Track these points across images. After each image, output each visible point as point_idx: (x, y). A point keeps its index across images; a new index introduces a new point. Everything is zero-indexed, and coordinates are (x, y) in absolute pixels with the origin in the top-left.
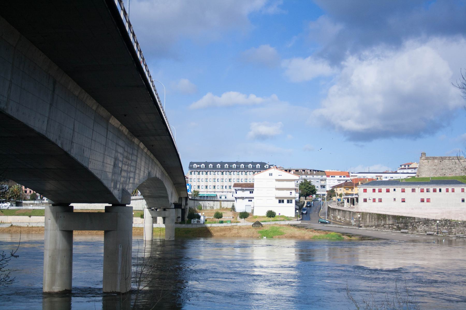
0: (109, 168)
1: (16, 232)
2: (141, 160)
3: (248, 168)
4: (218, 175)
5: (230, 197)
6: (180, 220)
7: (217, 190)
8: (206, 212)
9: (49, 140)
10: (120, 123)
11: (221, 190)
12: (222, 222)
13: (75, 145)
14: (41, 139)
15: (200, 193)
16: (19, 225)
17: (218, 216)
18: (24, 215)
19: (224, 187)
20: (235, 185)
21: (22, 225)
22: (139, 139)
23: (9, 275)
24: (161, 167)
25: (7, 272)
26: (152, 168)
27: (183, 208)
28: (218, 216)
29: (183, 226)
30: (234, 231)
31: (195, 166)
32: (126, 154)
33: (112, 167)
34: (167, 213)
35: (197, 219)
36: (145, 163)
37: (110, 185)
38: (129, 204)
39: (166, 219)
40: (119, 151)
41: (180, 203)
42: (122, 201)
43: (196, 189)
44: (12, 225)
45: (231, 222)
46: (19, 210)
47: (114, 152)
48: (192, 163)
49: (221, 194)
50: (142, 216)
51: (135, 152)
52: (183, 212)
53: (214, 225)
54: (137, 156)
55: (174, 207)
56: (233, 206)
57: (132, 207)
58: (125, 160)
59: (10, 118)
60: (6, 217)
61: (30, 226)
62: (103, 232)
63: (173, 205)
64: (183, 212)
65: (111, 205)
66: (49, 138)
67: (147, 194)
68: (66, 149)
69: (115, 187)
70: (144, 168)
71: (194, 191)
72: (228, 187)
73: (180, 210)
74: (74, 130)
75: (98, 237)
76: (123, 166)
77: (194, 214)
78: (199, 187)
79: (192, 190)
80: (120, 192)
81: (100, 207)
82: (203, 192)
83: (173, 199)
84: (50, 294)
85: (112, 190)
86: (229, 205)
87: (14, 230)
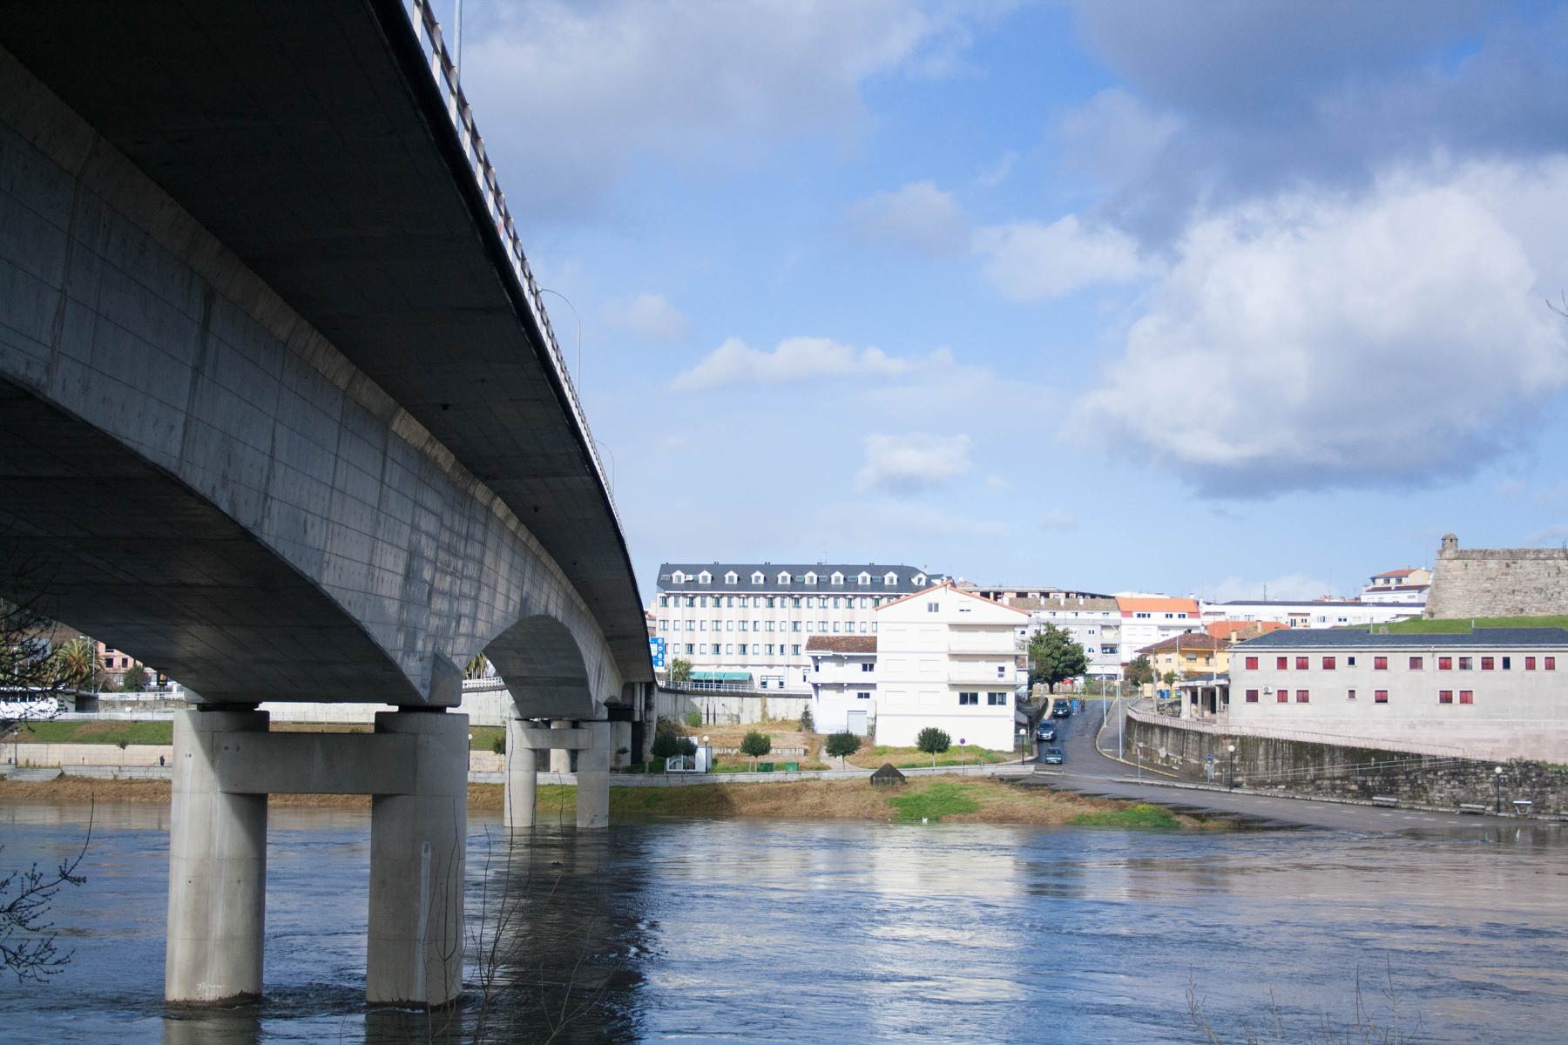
0: (391, 585)
4: (757, 609)
5: (795, 683)
6: (626, 760)
7: (750, 658)
9: (190, 492)
10: (427, 434)
11: (741, 659)
12: (768, 768)
13: (275, 507)
16: (87, 774)
18: (102, 740)
19: (777, 649)
20: (814, 643)
21: (96, 774)
22: (491, 487)
27: (637, 719)
28: (756, 745)
29: (639, 779)
30: (809, 800)
31: (679, 577)
32: (445, 537)
33: (399, 580)
34: (582, 737)
37: (391, 641)
38: (456, 706)
39: (581, 757)
40: (423, 526)
41: (628, 701)
43: (683, 656)
44: (62, 774)
45: (799, 768)
46: (86, 722)
47: (406, 530)
48: (667, 569)
49: (766, 671)
50: (500, 747)
51: (478, 532)
53: (741, 777)
54: (484, 544)
55: (606, 716)
56: (806, 714)
58: (443, 556)
59: (63, 415)
60: (44, 746)
61: (125, 776)
63: (605, 708)
65: (395, 709)
68: (246, 518)
69: (410, 649)
70: (502, 586)
71: (676, 663)
72: (788, 650)
73: (627, 728)
77: (673, 741)
78: (691, 647)
79: (669, 659)
80: (428, 664)
82: (704, 666)
83: (603, 688)
84: (189, 1011)
85: (398, 657)
86: (793, 710)
87: (69, 791)
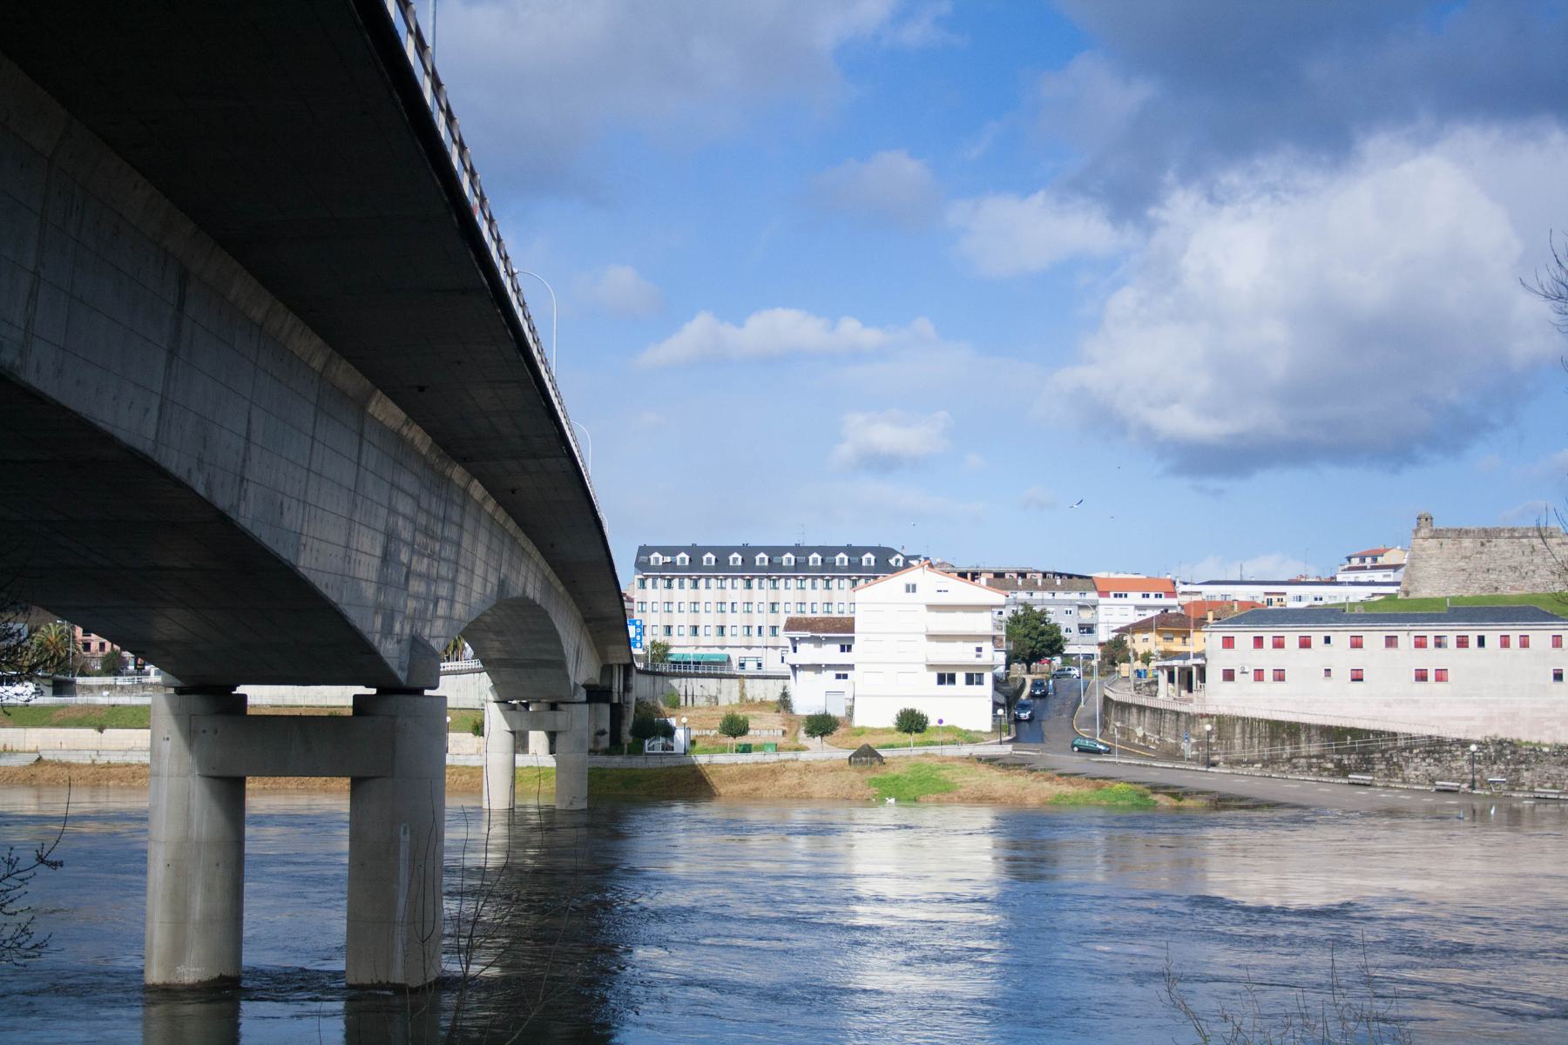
0: (367, 568)
1: (53, 783)
2: (475, 538)
3: (834, 568)
4: (735, 591)
5: (773, 664)
6: (605, 742)
7: (728, 640)
8: (692, 714)
9: (164, 474)
10: (404, 416)
11: (745, 641)
12: (746, 749)
13: (251, 490)
14: (139, 468)
15: (672, 651)
16: (64, 759)
17: (734, 727)
18: (80, 723)
19: (755, 631)
20: (792, 625)
21: (73, 759)
22: (468, 470)
23: (31, 928)
24: (543, 564)
25: (23, 919)
26: (511, 566)
27: (616, 700)
28: (734, 727)
29: (617, 761)
30: (788, 780)
31: (657, 558)
32: (422, 519)
33: (376, 562)
34: (560, 719)
35: (662, 740)
36: (489, 548)
37: (370, 625)
38: (434, 688)
39: (560, 739)
40: (401, 508)
41: (606, 683)
42: (409, 677)
43: (661, 638)
44: (40, 759)
45: (778, 749)
46: (63, 707)
47: (383, 512)
48: (645, 551)
49: (744, 652)
50: (478, 729)
51: (455, 513)
52: (617, 713)
53: (720, 759)
54: (461, 527)
55: (584, 698)
56: (785, 695)
57: (445, 698)
58: (420, 538)
59: (35, 397)
60: (21, 730)
61: (102, 760)
62: (345, 783)
63: (583, 690)
64: (617, 713)
65: (373, 691)
66: (165, 464)
67: (493, 655)
68: (222, 501)
69: (387, 631)
70: (484, 566)
71: (654, 645)
72: (766, 631)
73: (605, 710)
74: (248, 439)
75: (330, 798)
76: (415, 558)
77: (652, 723)
78: (668, 629)
79: (647, 641)
80: (405, 646)
81: (337, 697)
82: (683, 646)
83: (582, 670)
84: (169, 993)
85: (376, 639)
86: (772, 691)
87: (47, 776)
